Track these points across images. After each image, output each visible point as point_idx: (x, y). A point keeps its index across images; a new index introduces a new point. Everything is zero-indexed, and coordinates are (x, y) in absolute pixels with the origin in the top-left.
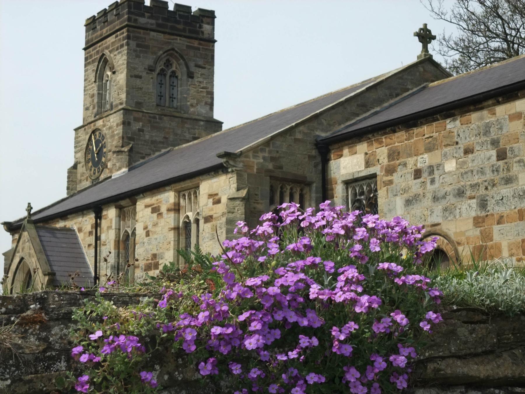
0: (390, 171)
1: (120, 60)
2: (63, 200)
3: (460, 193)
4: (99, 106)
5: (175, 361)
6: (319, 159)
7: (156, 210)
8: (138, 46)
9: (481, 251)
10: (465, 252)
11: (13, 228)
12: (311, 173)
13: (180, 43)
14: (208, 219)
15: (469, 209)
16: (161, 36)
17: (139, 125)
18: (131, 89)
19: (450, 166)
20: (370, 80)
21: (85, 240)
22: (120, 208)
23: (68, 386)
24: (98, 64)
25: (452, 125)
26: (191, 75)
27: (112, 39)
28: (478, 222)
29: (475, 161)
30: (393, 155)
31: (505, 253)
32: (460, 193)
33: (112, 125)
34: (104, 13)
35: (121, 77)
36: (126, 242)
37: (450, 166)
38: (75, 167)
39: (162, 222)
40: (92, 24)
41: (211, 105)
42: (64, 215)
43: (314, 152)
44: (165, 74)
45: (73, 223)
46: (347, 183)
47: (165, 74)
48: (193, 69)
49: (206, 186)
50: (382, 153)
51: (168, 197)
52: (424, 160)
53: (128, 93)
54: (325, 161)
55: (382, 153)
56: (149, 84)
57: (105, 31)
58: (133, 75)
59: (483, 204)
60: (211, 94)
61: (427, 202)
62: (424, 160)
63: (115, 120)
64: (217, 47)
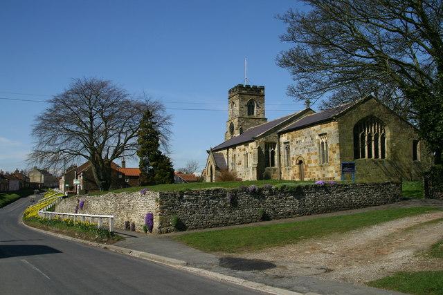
0: (292, 141)
1: (237, 102)
9: (323, 146)
10: (306, 161)
11: (208, 152)
15: (306, 151)
17: (242, 122)
19: (303, 141)
21: (225, 156)
23: (322, 89)
25: (303, 131)
28: (308, 154)
35: (238, 108)
42: (221, 150)
45: (223, 152)
46: (285, 143)
49: (250, 144)
51: (243, 146)
52: (299, 139)
54: (279, 137)
55: (290, 137)
57: (233, 94)
58: (241, 107)
61: (299, 149)
62: (299, 139)
63: (236, 120)
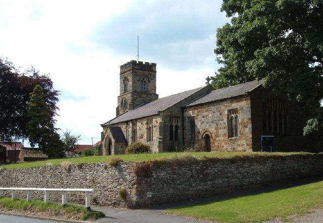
0: (198, 116)
1: (130, 78)
2: (115, 119)
3: (212, 122)
4: (124, 90)
5: (233, 57)
6: (181, 112)
7: (142, 124)
8: (135, 74)
12: (180, 115)
13: (146, 73)
14: (155, 127)
15: (214, 125)
16: (142, 72)
17: (136, 97)
18: (133, 87)
19: (210, 115)
20: (199, 89)
22: (133, 123)
24: (124, 80)
26: (150, 82)
27: (128, 72)
29: (215, 115)
30: (198, 112)
31: (221, 136)
32: (212, 122)
33: (129, 97)
34: (125, 65)
35: (131, 83)
36: (134, 132)
37: (210, 115)
38: (118, 107)
39: (144, 127)
40: (122, 67)
41: (155, 90)
43: (180, 110)
44: (143, 82)
47: (143, 82)
48: (150, 80)
50: (196, 111)
52: (205, 114)
53: (133, 87)
54: (183, 113)
56: (139, 84)
58: (134, 83)
59: (217, 125)
60: (155, 87)
61: (205, 124)
62: (205, 114)
63: (129, 95)
64: (157, 73)
